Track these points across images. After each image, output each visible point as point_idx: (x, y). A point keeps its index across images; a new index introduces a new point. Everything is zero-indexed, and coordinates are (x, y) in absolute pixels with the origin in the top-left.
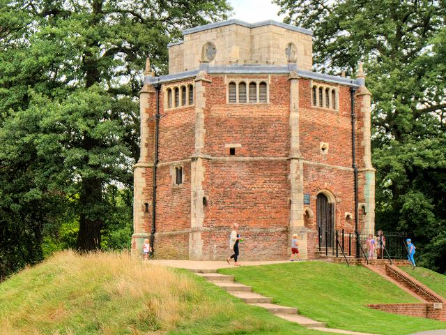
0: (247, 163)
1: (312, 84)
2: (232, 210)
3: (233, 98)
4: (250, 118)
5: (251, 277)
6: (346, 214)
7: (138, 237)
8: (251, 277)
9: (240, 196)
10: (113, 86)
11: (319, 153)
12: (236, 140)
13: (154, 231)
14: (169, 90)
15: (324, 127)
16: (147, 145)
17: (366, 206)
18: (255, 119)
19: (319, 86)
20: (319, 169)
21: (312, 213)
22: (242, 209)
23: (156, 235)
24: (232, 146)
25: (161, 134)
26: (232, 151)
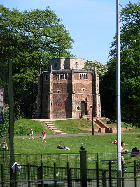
0: (62, 94)
1: (80, 74)
2: (58, 106)
3: (59, 79)
4: (62, 84)
5: (34, 122)
6: (90, 106)
7: (130, 153)
8: (34, 122)
9: (60, 103)
10: (99, 180)
11: (82, 91)
12: (59, 89)
13: (41, 112)
14: (45, 76)
15: (84, 84)
16: (40, 89)
17: (79, 117)
18: (64, 83)
19: (82, 74)
20: (82, 95)
21: (80, 106)
22: (61, 106)
23: (42, 112)
24: (59, 90)
25: (43, 87)
26: (59, 92)
